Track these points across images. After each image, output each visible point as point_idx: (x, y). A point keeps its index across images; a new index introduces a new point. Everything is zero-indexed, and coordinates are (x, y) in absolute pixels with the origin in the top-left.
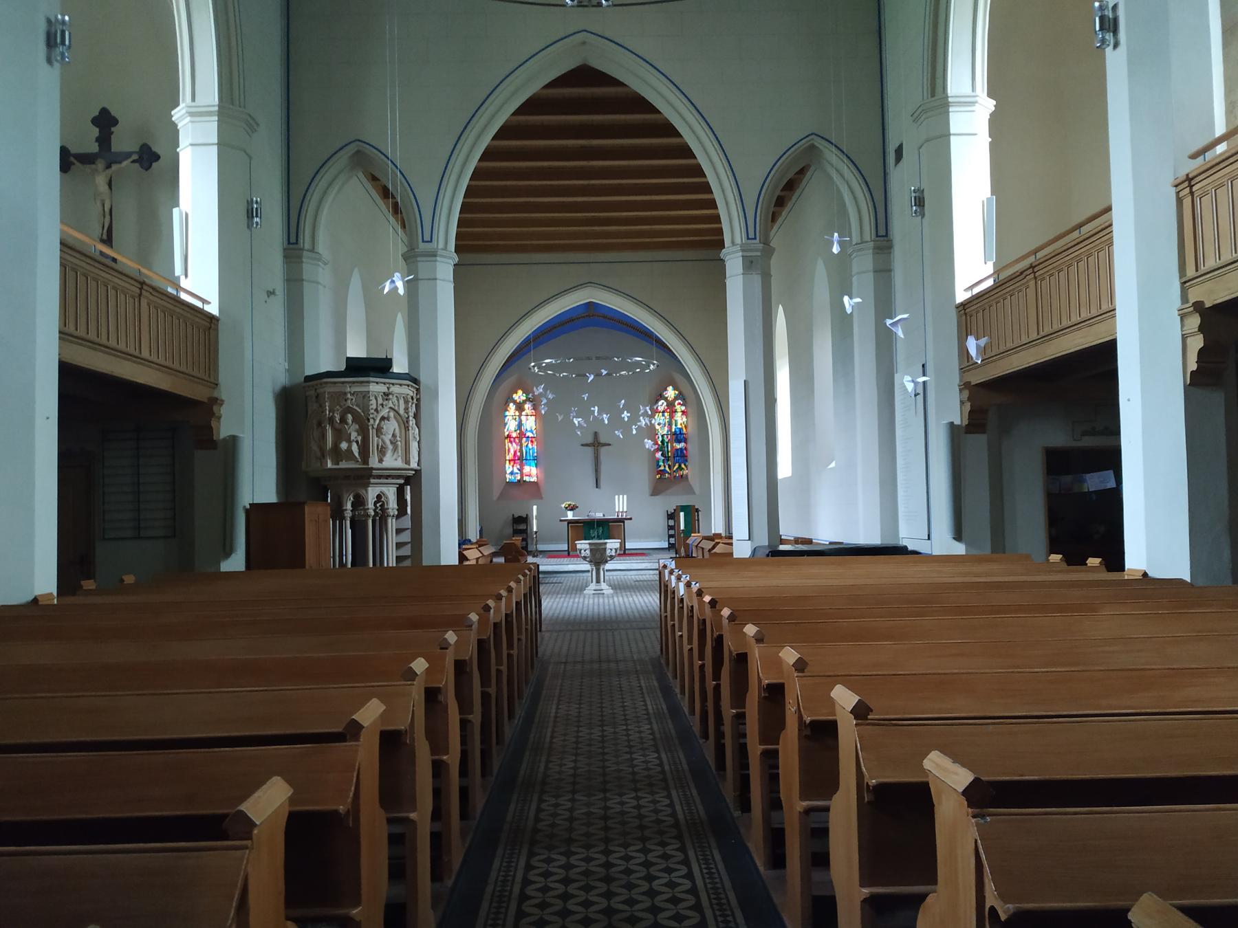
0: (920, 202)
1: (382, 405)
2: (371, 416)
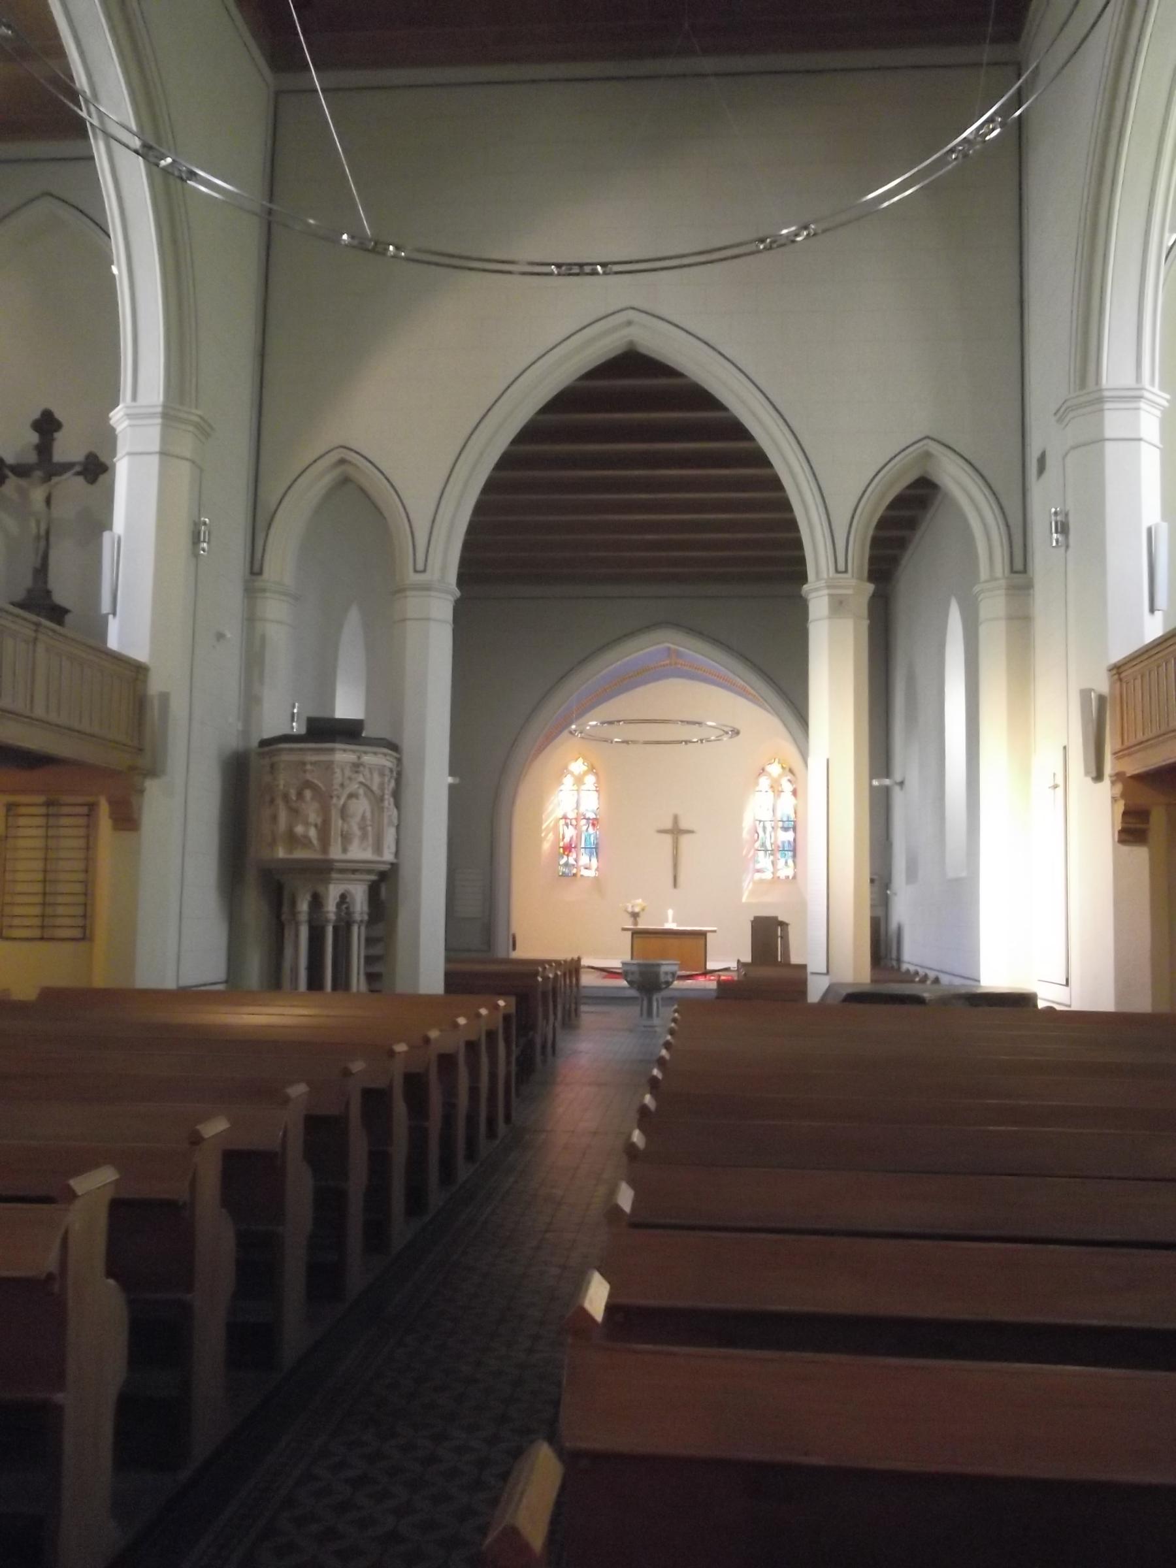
0: (1063, 528)
1: (350, 779)
2: (335, 793)
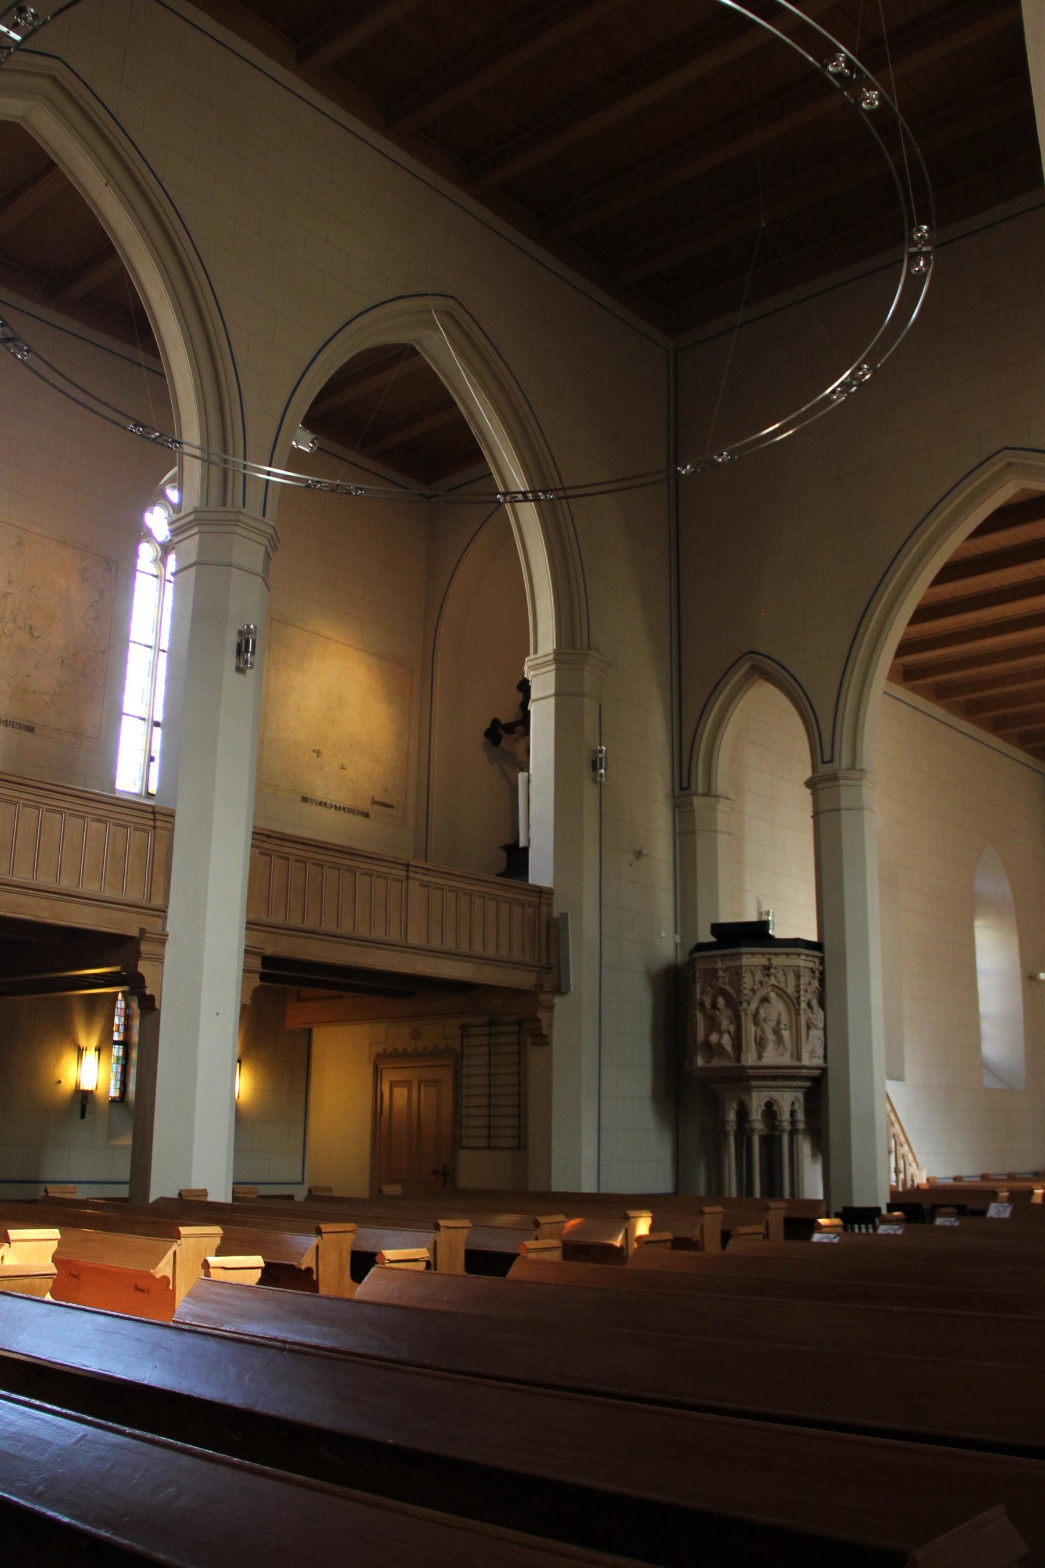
1: (761, 983)
